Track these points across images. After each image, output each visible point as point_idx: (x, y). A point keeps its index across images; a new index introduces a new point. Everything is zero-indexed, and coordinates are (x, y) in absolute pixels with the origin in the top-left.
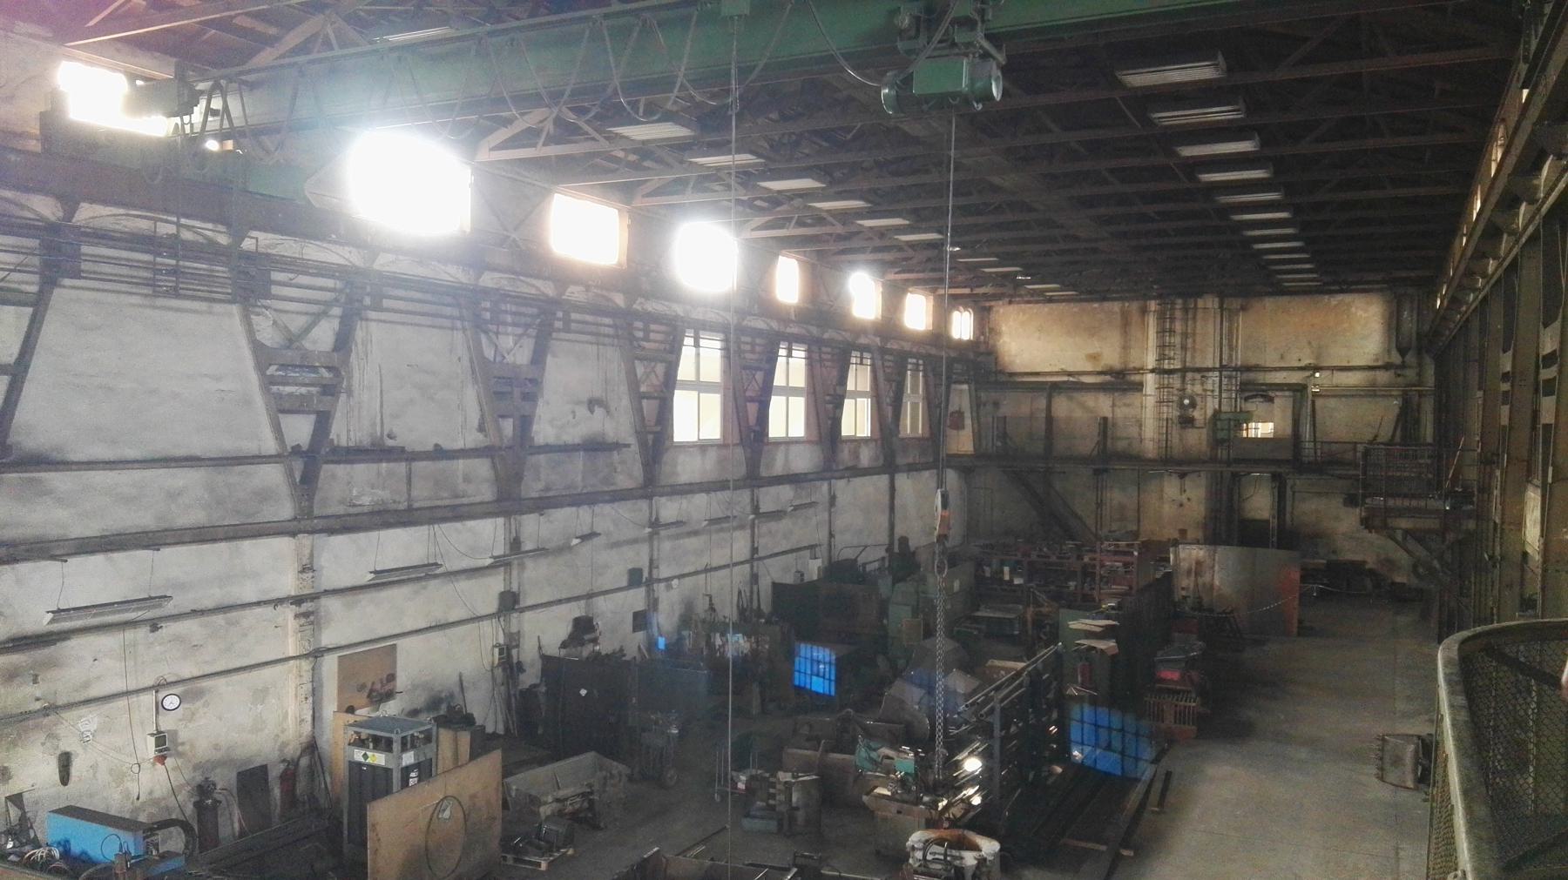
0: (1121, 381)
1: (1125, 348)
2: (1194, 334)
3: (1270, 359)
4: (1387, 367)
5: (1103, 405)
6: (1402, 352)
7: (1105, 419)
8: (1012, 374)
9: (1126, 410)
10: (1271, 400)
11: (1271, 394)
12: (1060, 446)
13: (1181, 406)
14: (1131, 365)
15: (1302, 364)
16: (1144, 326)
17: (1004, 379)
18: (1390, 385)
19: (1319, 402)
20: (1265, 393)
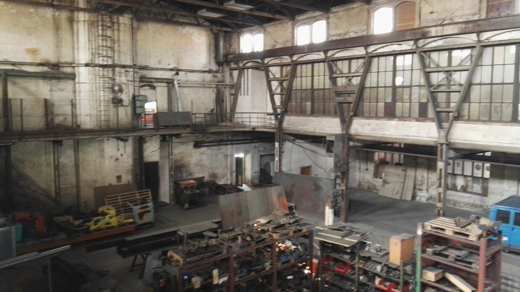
0: (56, 72)
1: (58, 46)
2: (119, 41)
3: (152, 63)
4: (210, 71)
5: (43, 89)
6: (219, 64)
7: (46, 100)
9: (61, 94)
11: (155, 84)
12: (16, 123)
13: (114, 91)
14: (63, 60)
20: (149, 83)
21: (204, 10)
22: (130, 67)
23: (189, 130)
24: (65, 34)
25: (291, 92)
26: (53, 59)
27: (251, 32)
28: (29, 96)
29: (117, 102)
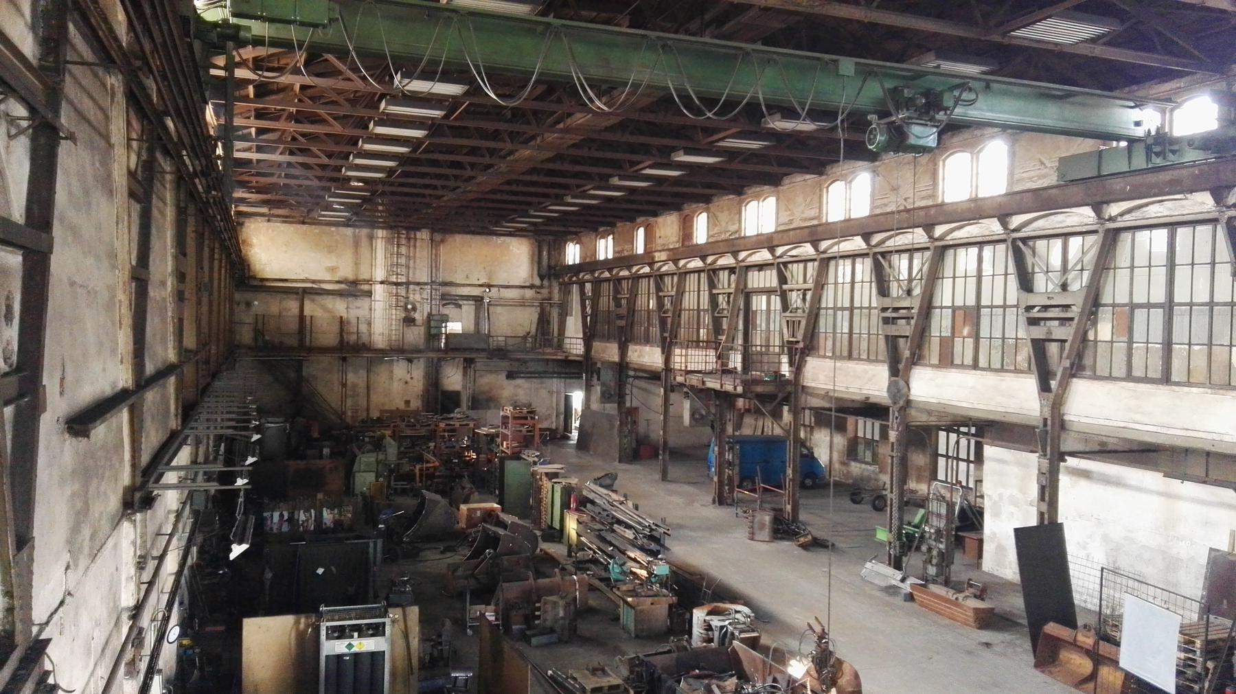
0: (355, 289)
1: (357, 264)
4: (532, 287)
5: (339, 307)
6: (542, 278)
8: (263, 280)
10: (460, 306)
13: (406, 309)
14: (361, 277)
15: (480, 282)
16: (372, 249)
17: (255, 283)
18: (533, 299)
19: (491, 309)
21: (681, 152)
22: (426, 284)
23: (484, 355)
24: (364, 250)
25: (817, 315)
26: (351, 277)
27: (757, 197)
28: (324, 314)
29: (409, 321)
